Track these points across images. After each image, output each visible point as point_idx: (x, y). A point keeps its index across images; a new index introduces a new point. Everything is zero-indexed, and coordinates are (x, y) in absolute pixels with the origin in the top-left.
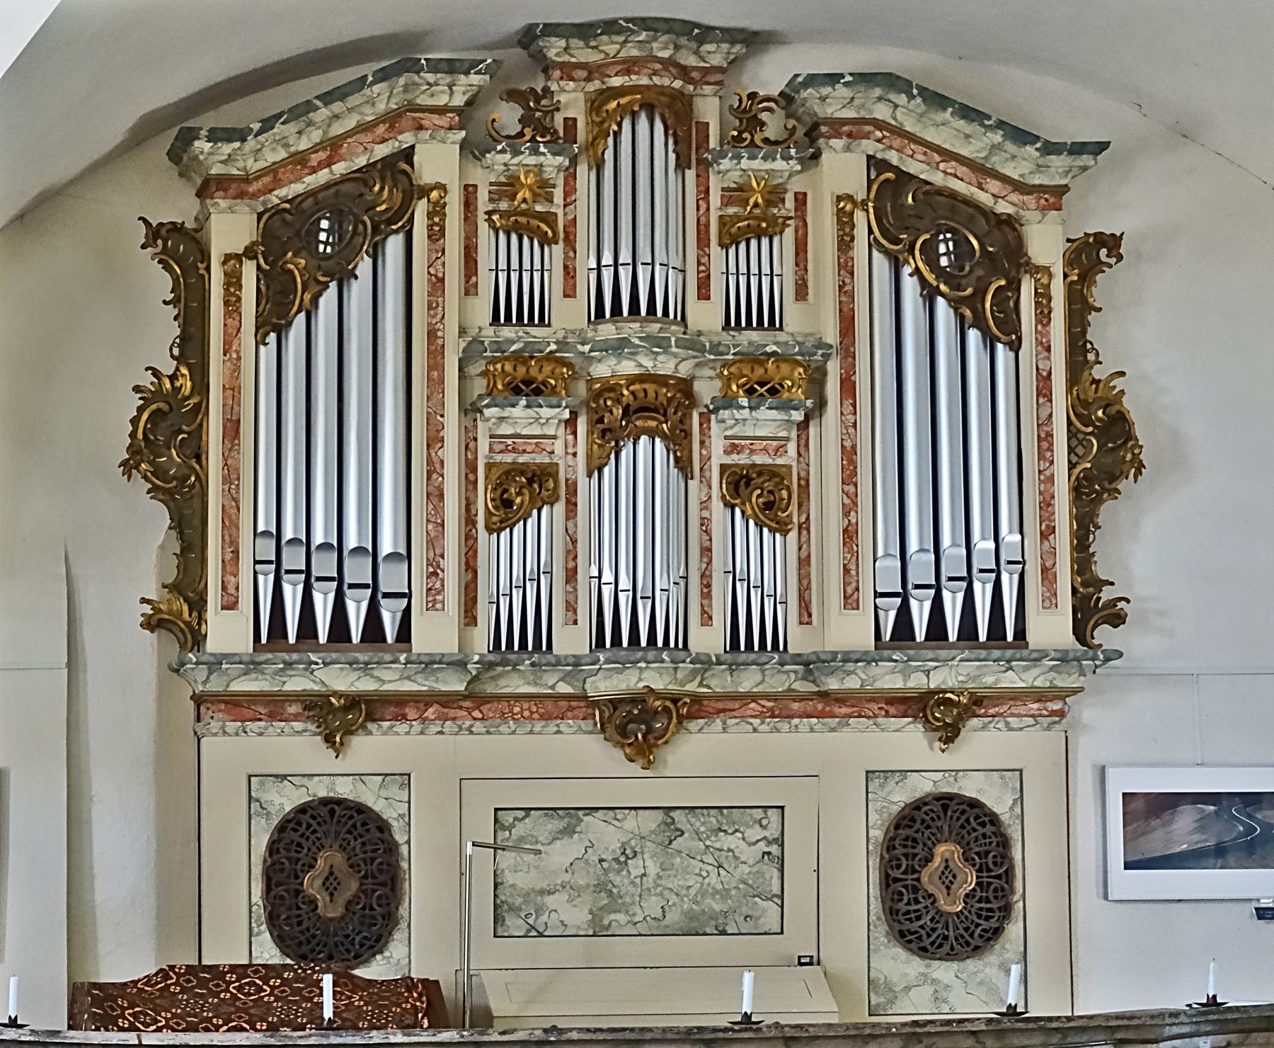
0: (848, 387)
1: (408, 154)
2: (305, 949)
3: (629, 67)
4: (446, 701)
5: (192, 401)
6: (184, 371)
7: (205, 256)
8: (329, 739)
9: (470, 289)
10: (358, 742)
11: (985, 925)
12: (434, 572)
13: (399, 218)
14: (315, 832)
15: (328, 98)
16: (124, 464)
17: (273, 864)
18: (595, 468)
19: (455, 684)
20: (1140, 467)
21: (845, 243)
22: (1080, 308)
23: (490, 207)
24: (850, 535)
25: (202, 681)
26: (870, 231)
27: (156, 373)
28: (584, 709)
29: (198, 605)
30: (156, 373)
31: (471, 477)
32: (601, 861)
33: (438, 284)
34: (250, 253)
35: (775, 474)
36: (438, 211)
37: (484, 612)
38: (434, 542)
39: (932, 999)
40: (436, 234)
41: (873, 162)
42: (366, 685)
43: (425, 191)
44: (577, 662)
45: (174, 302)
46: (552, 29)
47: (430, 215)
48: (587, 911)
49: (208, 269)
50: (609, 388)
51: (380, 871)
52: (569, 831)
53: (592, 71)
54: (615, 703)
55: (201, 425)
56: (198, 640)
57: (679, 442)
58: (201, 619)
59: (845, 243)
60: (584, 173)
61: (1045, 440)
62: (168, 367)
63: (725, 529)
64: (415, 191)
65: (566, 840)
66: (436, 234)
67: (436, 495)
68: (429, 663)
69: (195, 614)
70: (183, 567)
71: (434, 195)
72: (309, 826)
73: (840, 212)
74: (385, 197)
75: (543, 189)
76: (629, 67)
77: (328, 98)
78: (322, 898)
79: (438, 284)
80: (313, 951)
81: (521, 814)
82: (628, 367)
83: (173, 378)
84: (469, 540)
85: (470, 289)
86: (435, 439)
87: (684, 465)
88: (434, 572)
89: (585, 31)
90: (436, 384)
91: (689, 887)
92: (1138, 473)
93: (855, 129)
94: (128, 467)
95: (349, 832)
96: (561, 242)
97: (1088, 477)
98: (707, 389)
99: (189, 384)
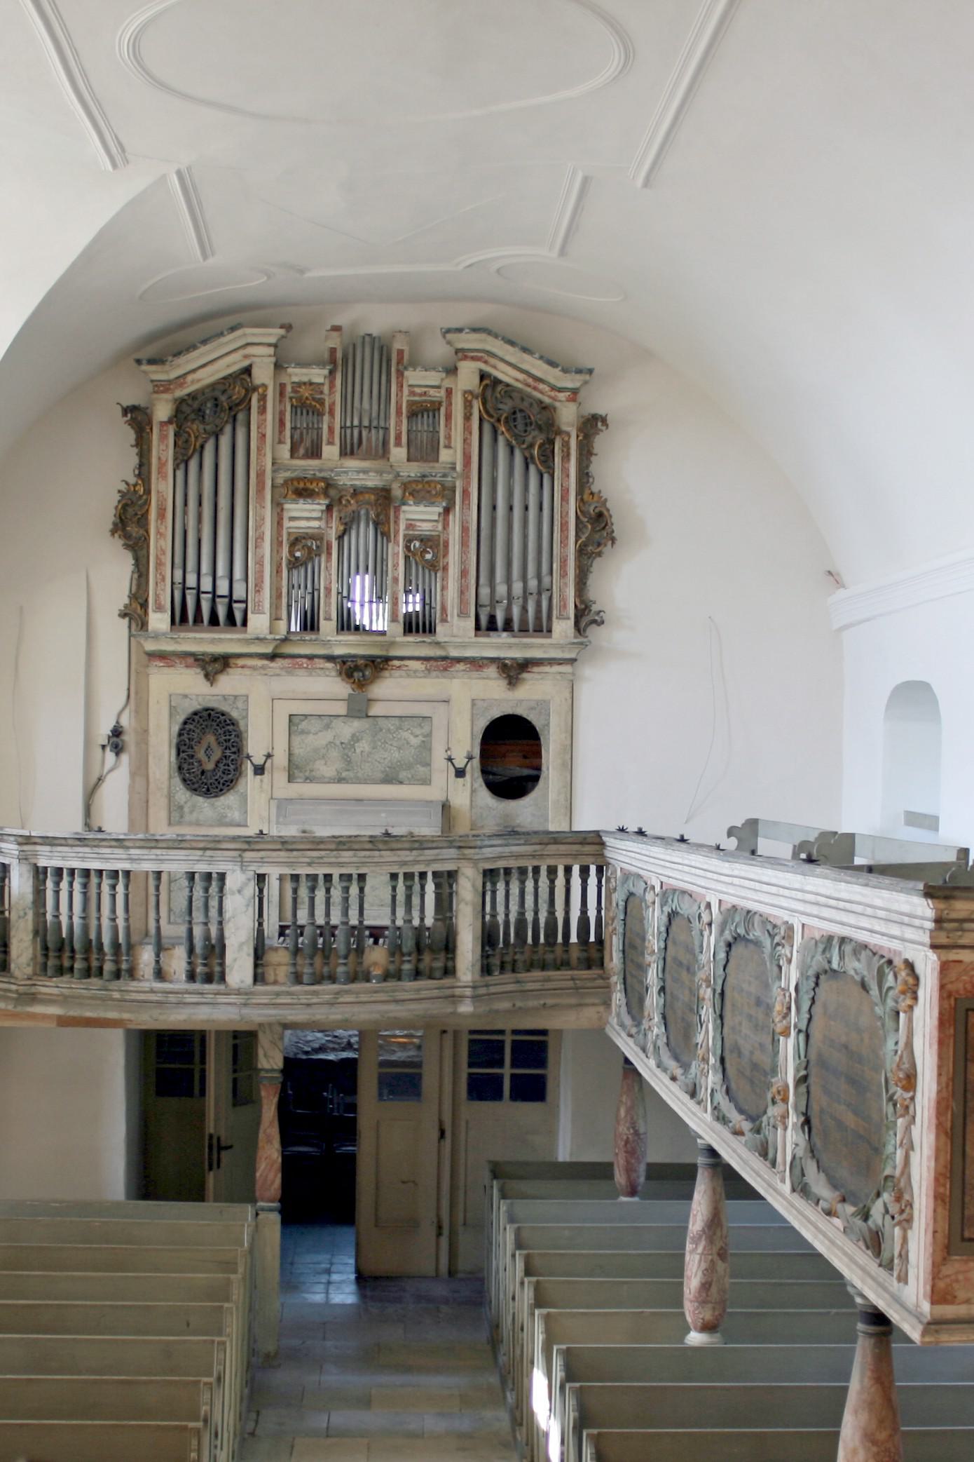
2: (196, 786)
5: (145, 497)
6: (140, 482)
7: (150, 423)
8: (207, 676)
11: (192, 727)
14: (202, 725)
16: (787, 922)
17: (181, 741)
20: (613, 540)
22: (586, 452)
23: (292, 395)
25: (150, 646)
26: (480, 411)
27: (127, 483)
29: (144, 605)
30: (127, 483)
31: (280, 539)
32: (342, 743)
34: (170, 422)
36: (263, 398)
39: (231, 1071)
43: (255, 389)
45: (136, 445)
47: (259, 401)
48: (334, 769)
49: (151, 429)
51: (233, 746)
52: (327, 727)
55: (147, 510)
56: (143, 625)
58: (146, 613)
61: (564, 526)
62: (132, 480)
63: (104, 115)
69: (143, 610)
70: (139, 586)
71: (260, 390)
72: (198, 722)
73: (466, 400)
74: (238, 392)
78: (204, 759)
80: (200, 787)
81: (303, 717)
83: (135, 485)
91: (385, 759)
92: (613, 543)
94: (113, 532)
95: (218, 725)
96: (327, 415)
97: (585, 545)
99: (142, 489)
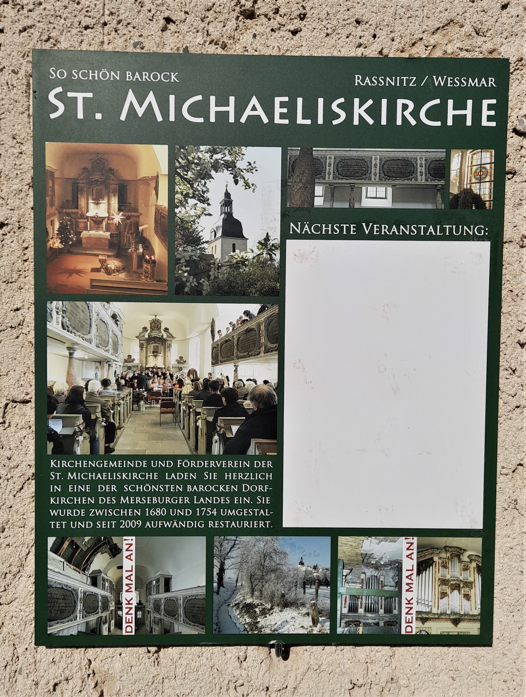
0: (475, 586)
1: (433, 558)
3: (455, 551)
4: (436, 619)
9: (439, 573)
10: (426, 623)
12: (435, 603)
13: (432, 565)
15: (425, 550)
18: (451, 593)
19: (437, 616)
21: (474, 574)
24: (475, 602)
28: (272, 389)
33: (436, 572)
35: (468, 595)
36: (436, 564)
37: (440, 608)
38: (435, 600)
40: (436, 566)
41: (477, 564)
42: (427, 616)
44: (449, 614)
46: (447, 547)
50: (452, 585)
53: (451, 552)
54: (453, 619)
57: (459, 591)
59: (474, 572)
60: (450, 562)
64: (434, 562)
65: (380, 50)
66: (436, 566)
67: (435, 595)
68: (434, 614)
75: (446, 563)
76: (455, 551)
77: (425, 550)
79: (436, 572)
82: (454, 582)
84: (438, 600)
85: (439, 573)
86: (435, 589)
87: (459, 593)
88: (435, 603)
89: (451, 547)
90: (435, 582)
93: (475, 560)
98: (461, 585)
